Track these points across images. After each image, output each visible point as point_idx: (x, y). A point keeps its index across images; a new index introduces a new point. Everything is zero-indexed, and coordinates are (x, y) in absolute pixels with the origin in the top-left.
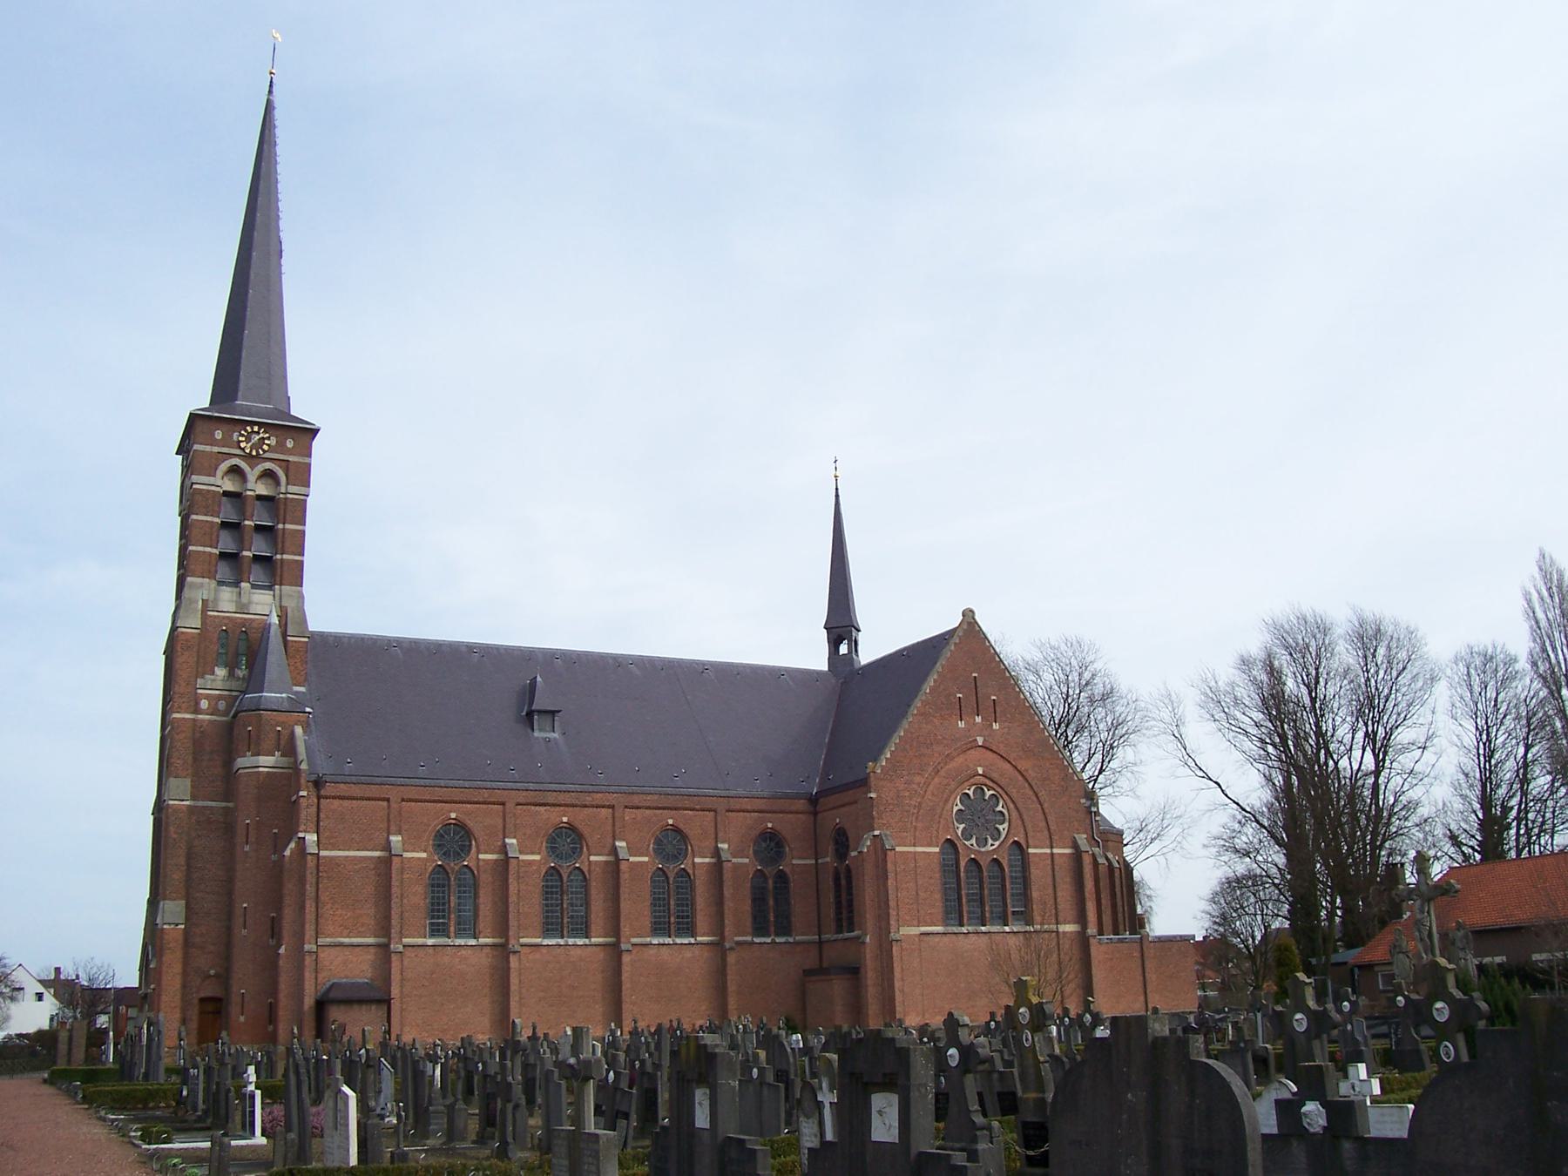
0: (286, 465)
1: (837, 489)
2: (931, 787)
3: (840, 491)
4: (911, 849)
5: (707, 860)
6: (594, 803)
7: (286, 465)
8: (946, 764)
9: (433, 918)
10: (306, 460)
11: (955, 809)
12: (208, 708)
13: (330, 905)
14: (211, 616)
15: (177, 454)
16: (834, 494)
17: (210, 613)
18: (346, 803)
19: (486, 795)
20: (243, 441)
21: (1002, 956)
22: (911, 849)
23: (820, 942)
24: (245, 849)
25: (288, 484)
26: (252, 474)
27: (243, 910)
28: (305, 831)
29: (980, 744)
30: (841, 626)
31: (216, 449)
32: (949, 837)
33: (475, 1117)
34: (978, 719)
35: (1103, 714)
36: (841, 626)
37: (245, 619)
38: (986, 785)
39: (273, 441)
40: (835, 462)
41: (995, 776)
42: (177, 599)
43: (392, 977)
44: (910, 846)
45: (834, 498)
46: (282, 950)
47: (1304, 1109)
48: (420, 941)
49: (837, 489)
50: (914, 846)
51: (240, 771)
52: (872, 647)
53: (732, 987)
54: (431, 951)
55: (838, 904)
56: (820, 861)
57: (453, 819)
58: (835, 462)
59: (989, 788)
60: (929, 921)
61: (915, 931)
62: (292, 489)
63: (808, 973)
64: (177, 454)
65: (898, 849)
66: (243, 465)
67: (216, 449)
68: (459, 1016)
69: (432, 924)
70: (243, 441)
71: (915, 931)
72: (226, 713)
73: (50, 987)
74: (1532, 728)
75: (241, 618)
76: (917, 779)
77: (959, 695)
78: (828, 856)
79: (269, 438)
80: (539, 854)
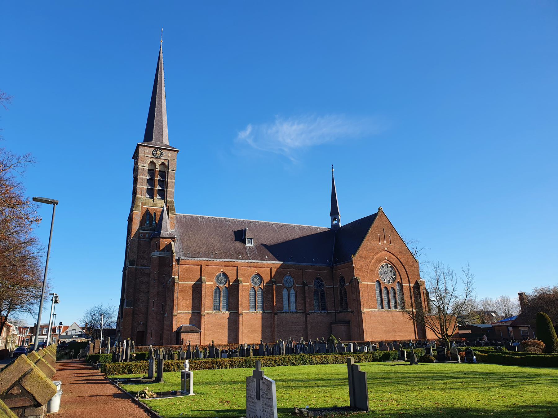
2: (371, 263)
4: (366, 283)
5: (300, 285)
6: (265, 266)
8: (376, 256)
9: (215, 304)
11: (379, 271)
12: (143, 237)
13: (182, 300)
14: (144, 208)
15: (132, 158)
16: (332, 175)
17: (143, 206)
18: (188, 266)
19: (232, 264)
21: (25, 253)
22: (366, 283)
23: (335, 313)
24: (154, 282)
27: (152, 302)
28: (174, 276)
29: (386, 250)
30: (334, 213)
32: (378, 280)
33: (239, 386)
34: (385, 242)
36: (334, 213)
37: (155, 209)
38: (388, 263)
40: (332, 166)
41: (391, 260)
42: (132, 203)
43: (202, 323)
44: (366, 282)
46: (166, 315)
48: (211, 312)
50: (367, 282)
51: (153, 256)
52: (344, 220)
53: (309, 328)
54: (214, 315)
55: (341, 301)
56: (334, 287)
57: (222, 271)
58: (332, 166)
59: (389, 264)
60: (373, 307)
61: (369, 310)
63: (332, 323)
64: (132, 158)
65: (363, 283)
66: (155, 160)
68: (223, 337)
69: (215, 306)
71: (369, 310)
72: (148, 238)
75: (154, 208)
76: (367, 260)
77: (379, 234)
78: (337, 285)
80: (249, 283)
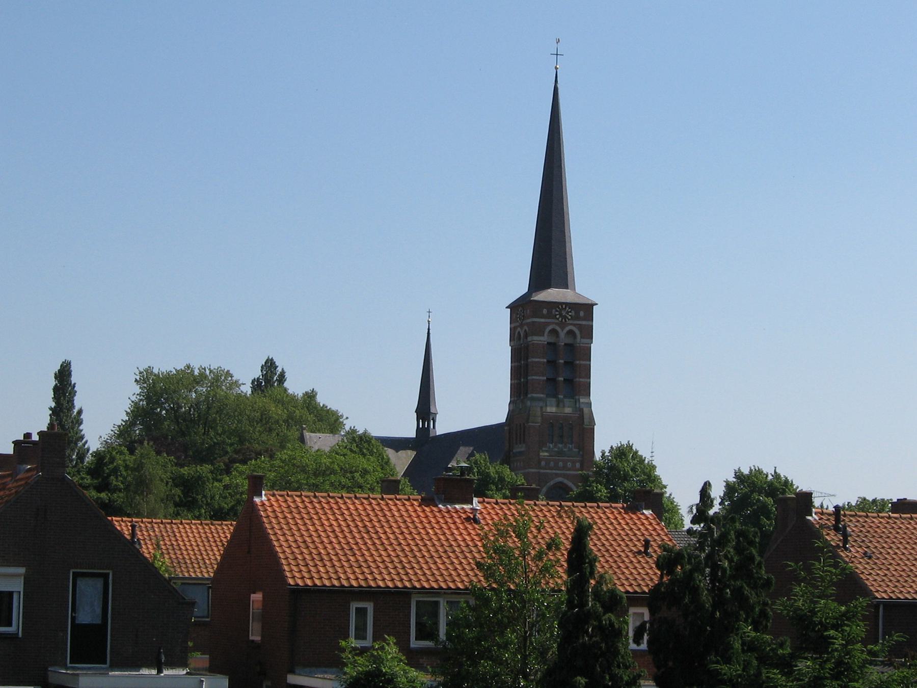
0: (580, 327)
1: (429, 329)
3: (430, 331)
7: (580, 327)
10: (589, 323)
20: (557, 315)
25: (581, 338)
26: (562, 334)
30: (425, 410)
31: (543, 320)
35: (179, 387)
36: (425, 410)
39: (573, 313)
45: (427, 335)
47: (392, 640)
49: (429, 329)
62: (583, 340)
67: (543, 320)
70: (557, 315)
73: (654, 588)
74: (543, 629)
79: (570, 312)
